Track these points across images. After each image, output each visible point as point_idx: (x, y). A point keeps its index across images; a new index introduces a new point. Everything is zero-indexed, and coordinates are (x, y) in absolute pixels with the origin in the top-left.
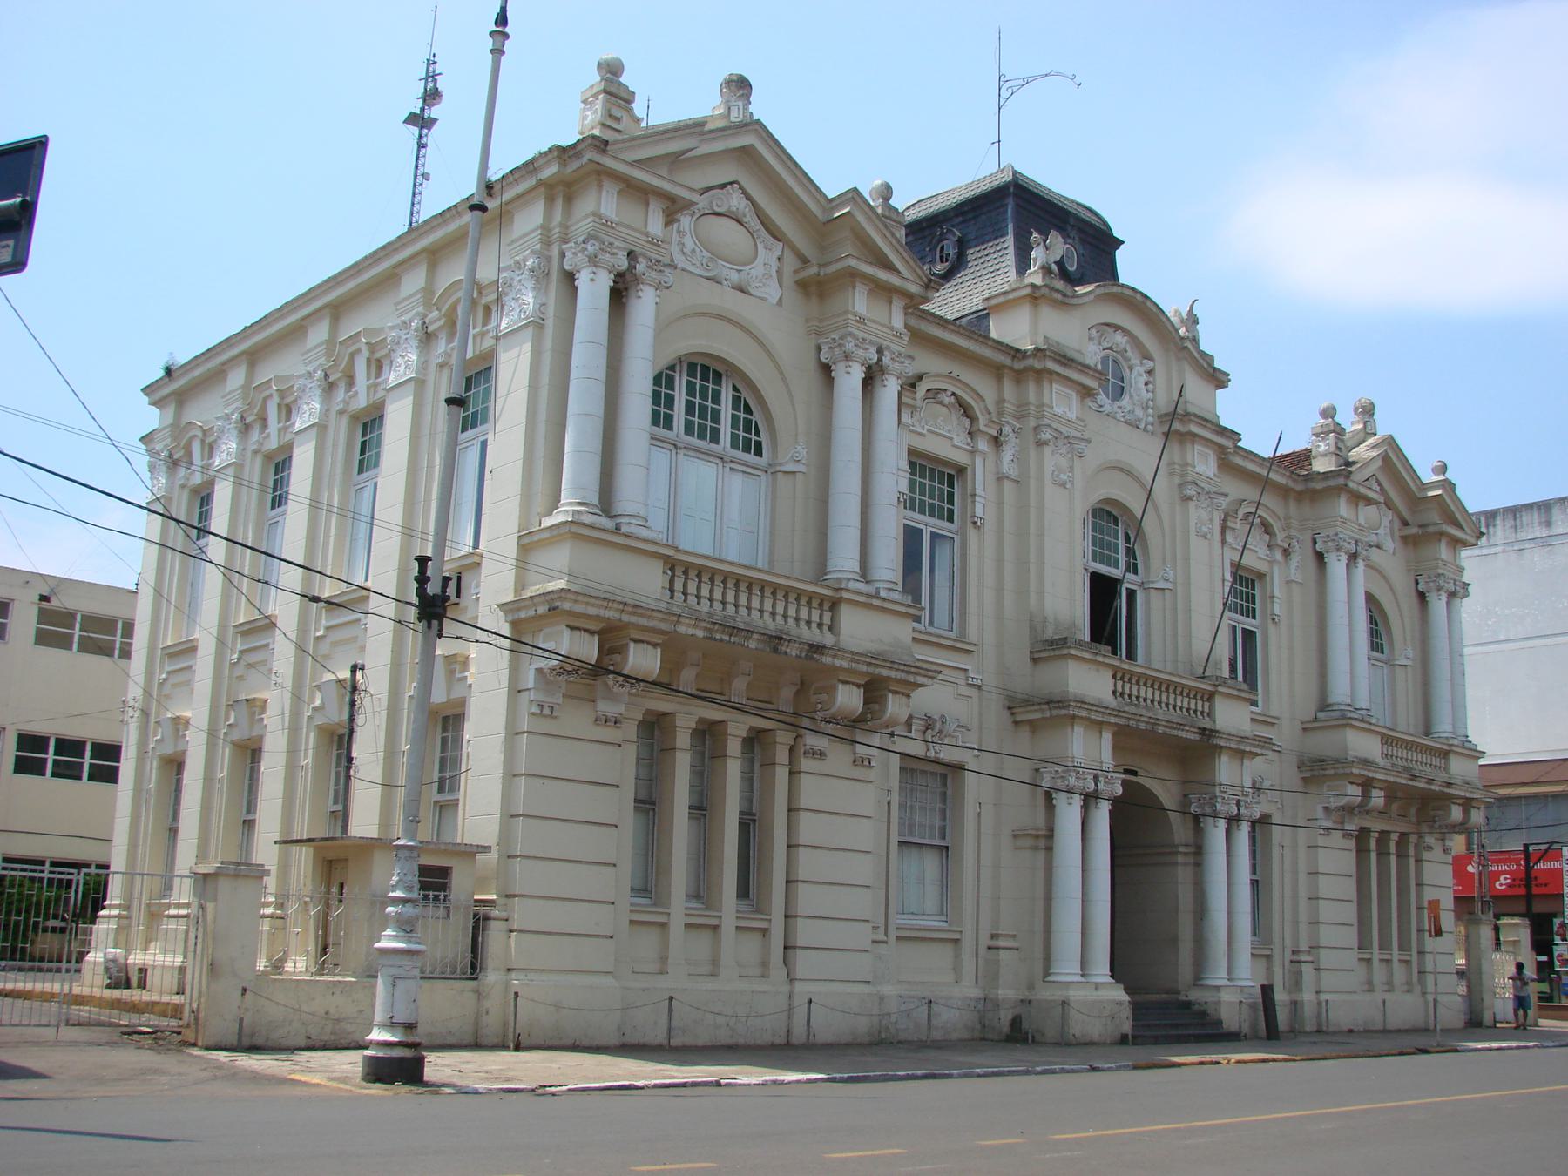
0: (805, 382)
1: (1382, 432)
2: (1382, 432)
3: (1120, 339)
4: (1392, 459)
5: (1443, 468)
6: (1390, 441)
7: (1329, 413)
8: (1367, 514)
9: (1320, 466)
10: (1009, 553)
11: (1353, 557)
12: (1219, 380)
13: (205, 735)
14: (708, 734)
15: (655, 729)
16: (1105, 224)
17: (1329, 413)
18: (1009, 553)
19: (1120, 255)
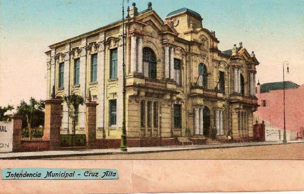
0: (161, 51)
1: (243, 48)
2: (243, 48)
3: (204, 37)
4: (246, 52)
5: (253, 52)
6: (245, 50)
7: (235, 45)
8: (241, 61)
9: (234, 54)
10: (127, 56)
11: (238, 69)
12: (218, 42)
13: (282, 80)
14: (149, 103)
15: (143, 104)
16: (199, 15)
17: (235, 45)
18: (127, 56)
19: (203, 21)
